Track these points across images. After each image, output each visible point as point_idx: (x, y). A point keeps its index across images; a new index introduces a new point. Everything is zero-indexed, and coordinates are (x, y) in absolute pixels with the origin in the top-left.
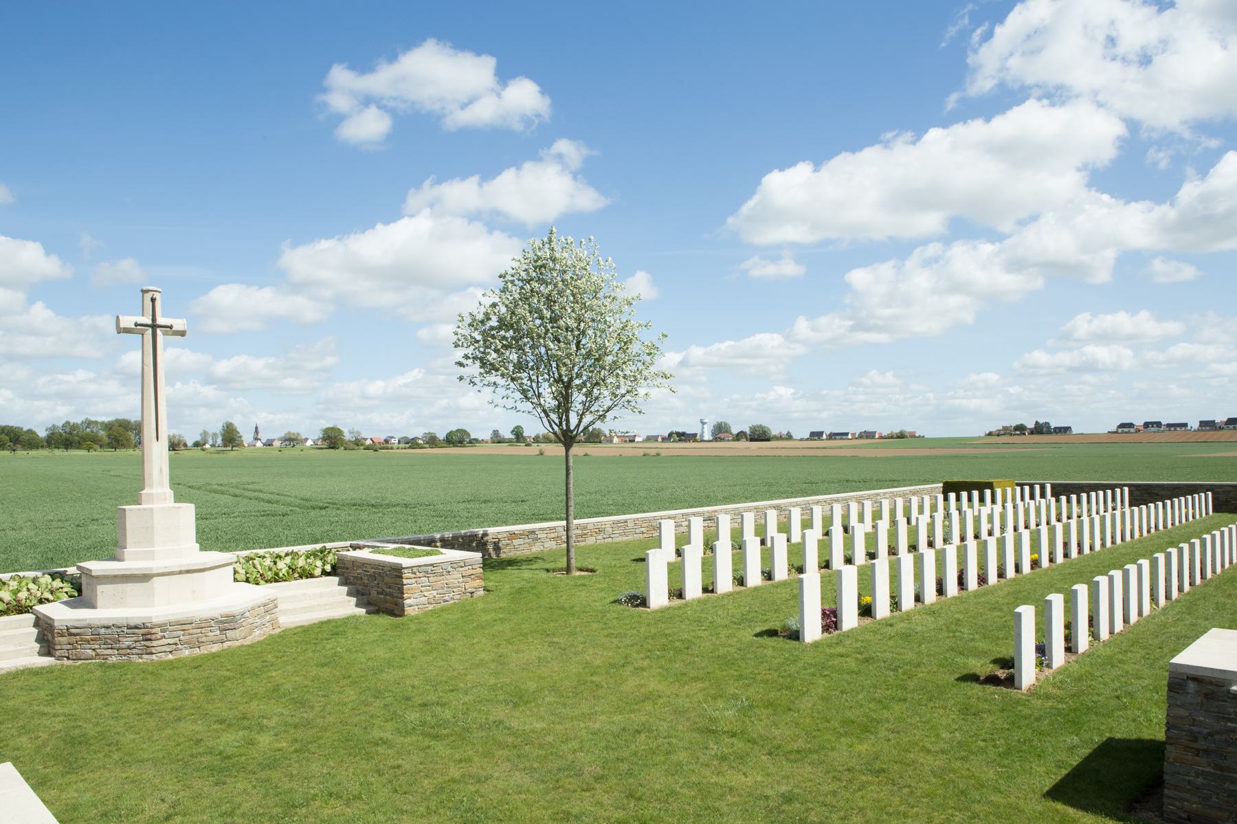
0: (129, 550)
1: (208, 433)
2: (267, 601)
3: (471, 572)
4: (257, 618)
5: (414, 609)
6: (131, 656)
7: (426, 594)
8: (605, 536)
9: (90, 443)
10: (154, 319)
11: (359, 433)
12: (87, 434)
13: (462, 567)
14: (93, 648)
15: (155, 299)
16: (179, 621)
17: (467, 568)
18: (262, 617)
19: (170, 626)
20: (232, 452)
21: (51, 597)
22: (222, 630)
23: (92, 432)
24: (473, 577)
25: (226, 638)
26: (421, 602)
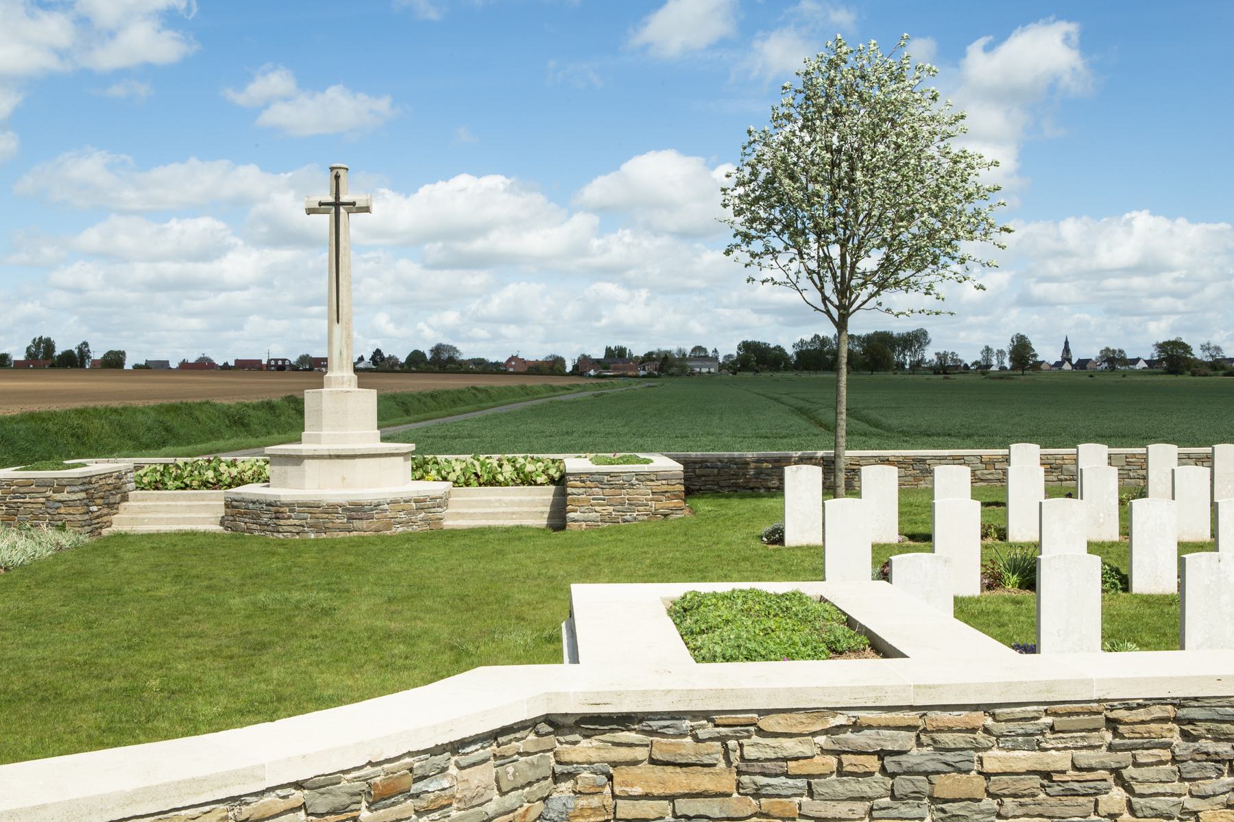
1: (991, 350)
3: (665, 488)
5: (580, 526)
7: (597, 508)
8: (1062, 477)
11: (1218, 349)
13: (652, 481)
15: (339, 177)
16: (306, 503)
17: (659, 483)
18: (414, 514)
20: (1023, 377)
22: (350, 518)
24: (668, 494)
26: (590, 518)
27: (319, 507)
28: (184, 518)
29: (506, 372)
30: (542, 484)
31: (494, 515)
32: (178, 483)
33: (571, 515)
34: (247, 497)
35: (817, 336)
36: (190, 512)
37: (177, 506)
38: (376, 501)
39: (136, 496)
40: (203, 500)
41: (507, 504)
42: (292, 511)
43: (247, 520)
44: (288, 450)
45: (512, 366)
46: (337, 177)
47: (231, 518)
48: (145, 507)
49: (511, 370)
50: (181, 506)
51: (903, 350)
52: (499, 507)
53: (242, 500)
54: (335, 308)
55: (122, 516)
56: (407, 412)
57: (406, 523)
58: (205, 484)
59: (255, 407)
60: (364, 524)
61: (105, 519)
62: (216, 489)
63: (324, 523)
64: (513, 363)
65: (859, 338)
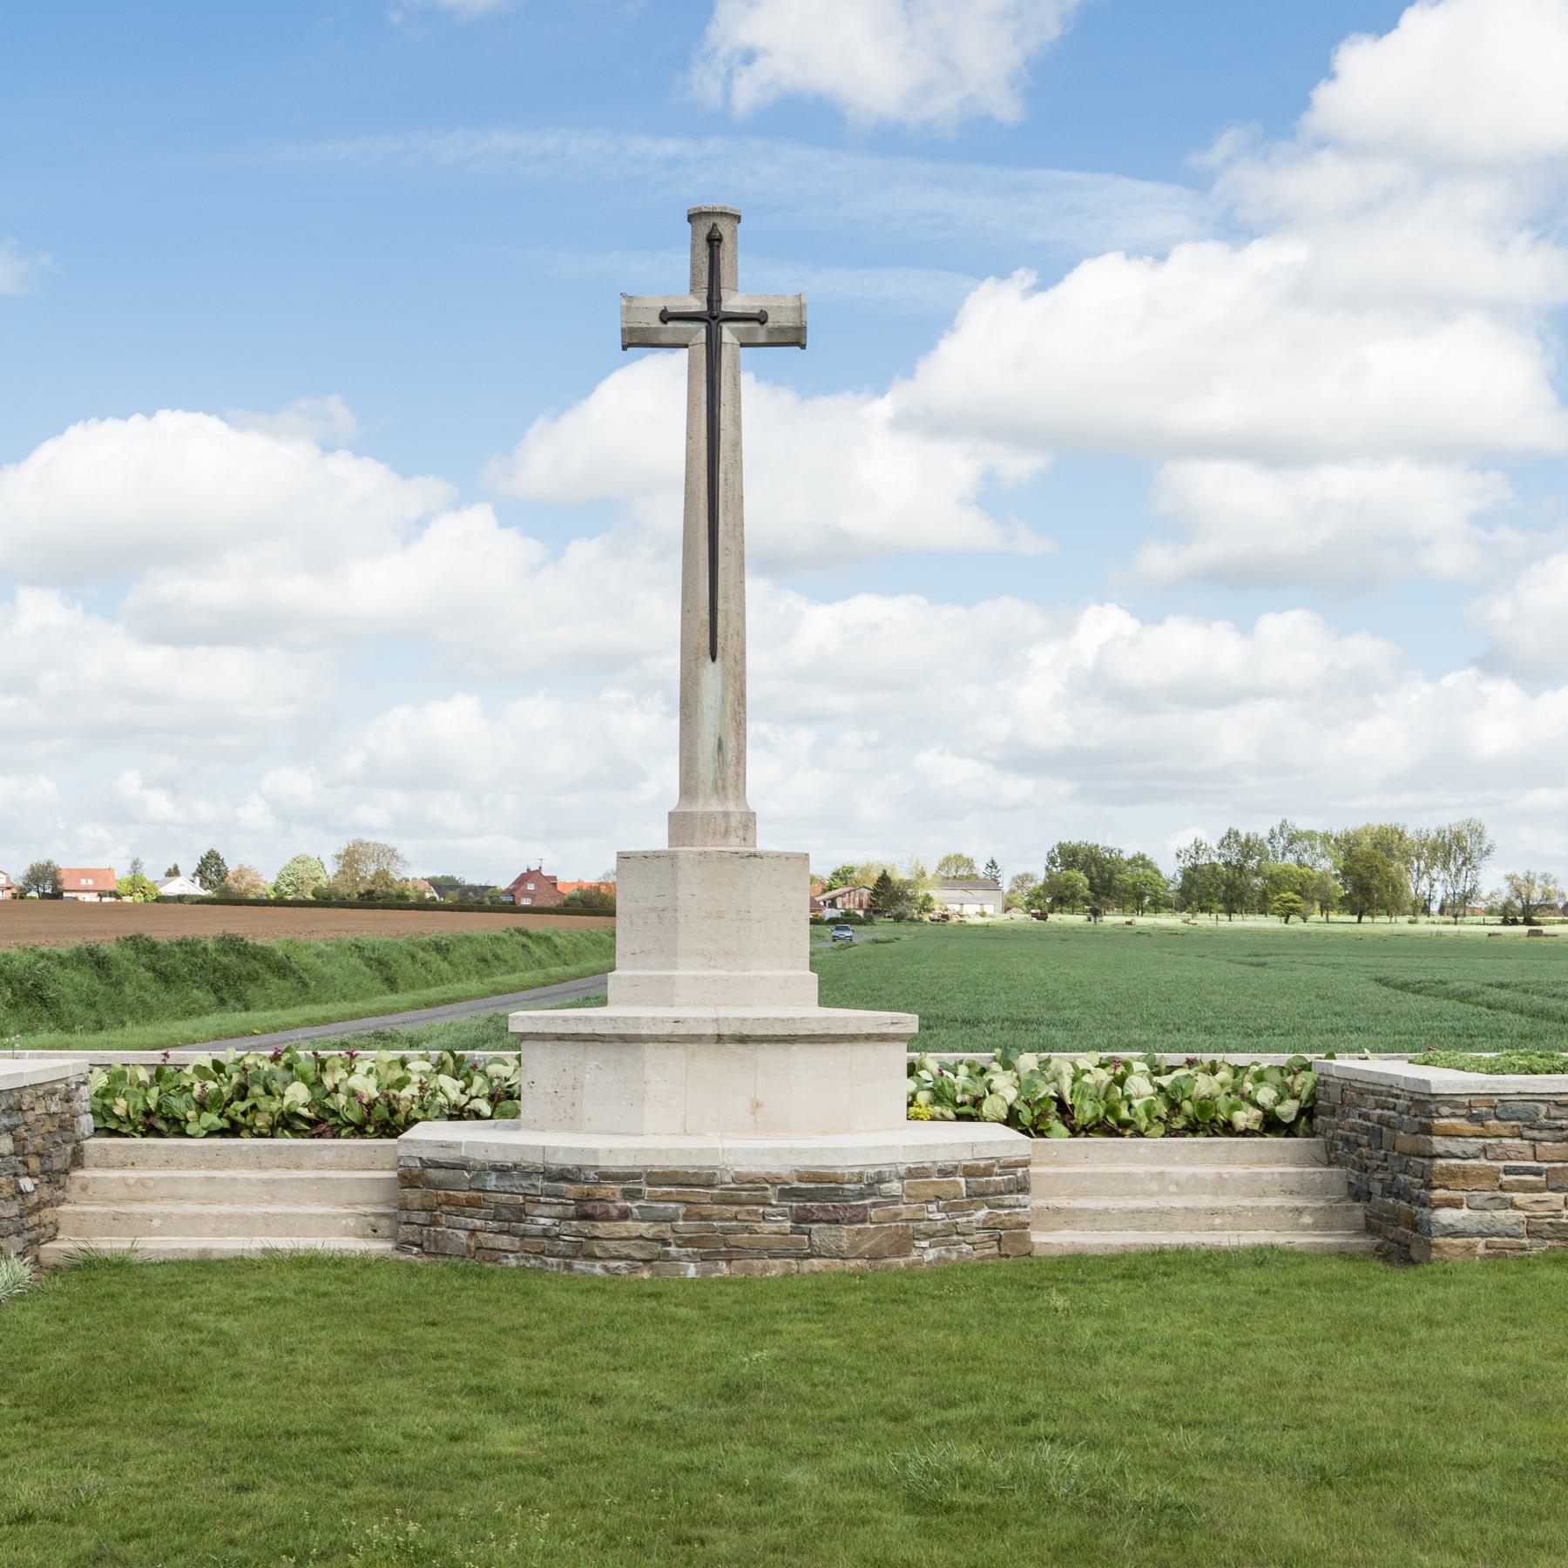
0: (623, 973)
2: (982, 1164)
4: (932, 1207)
5: (1469, 1249)
6: (550, 1260)
9: (1291, 895)
10: (713, 298)
12: (1287, 871)
14: (471, 1227)
15: (720, 240)
16: (814, 1174)
19: (649, 1184)
21: (486, 1109)
22: (801, 1218)
23: (1300, 864)
25: (811, 1246)
27: (710, 1186)
28: (266, 1217)
29: (512, 908)
30: (1246, 1133)
31: (1163, 1217)
32: (211, 1119)
33: (1445, 1216)
34: (479, 1156)
35: (1232, 835)
36: (274, 1199)
37: (234, 1180)
38: (871, 1171)
39: (105, 1151)
40: (298, 1167)
41: (1182, 1188)
42: (631, 1195)
43: (478, 1223)
44: (588, 1019)
45: (528, 894)
46: (714, 241)
47: (422, 1217)
48: (142, 1183)
49: (526, 902)
50: (248, 1180)
51: (1429, 867)
52: (1159, 1193)
53: (461, 1166)
54: (705, 615)
55: (78, 1208)
56: (391, 983)
57: (940, 1236)
58: (287, 1123)
59: (62, 962)
60: (844, 1235)
61: (47, 1214)
62: (320, 1135)
63: (726, 1231)
64: (531, 887)
65: (1326, 838)
